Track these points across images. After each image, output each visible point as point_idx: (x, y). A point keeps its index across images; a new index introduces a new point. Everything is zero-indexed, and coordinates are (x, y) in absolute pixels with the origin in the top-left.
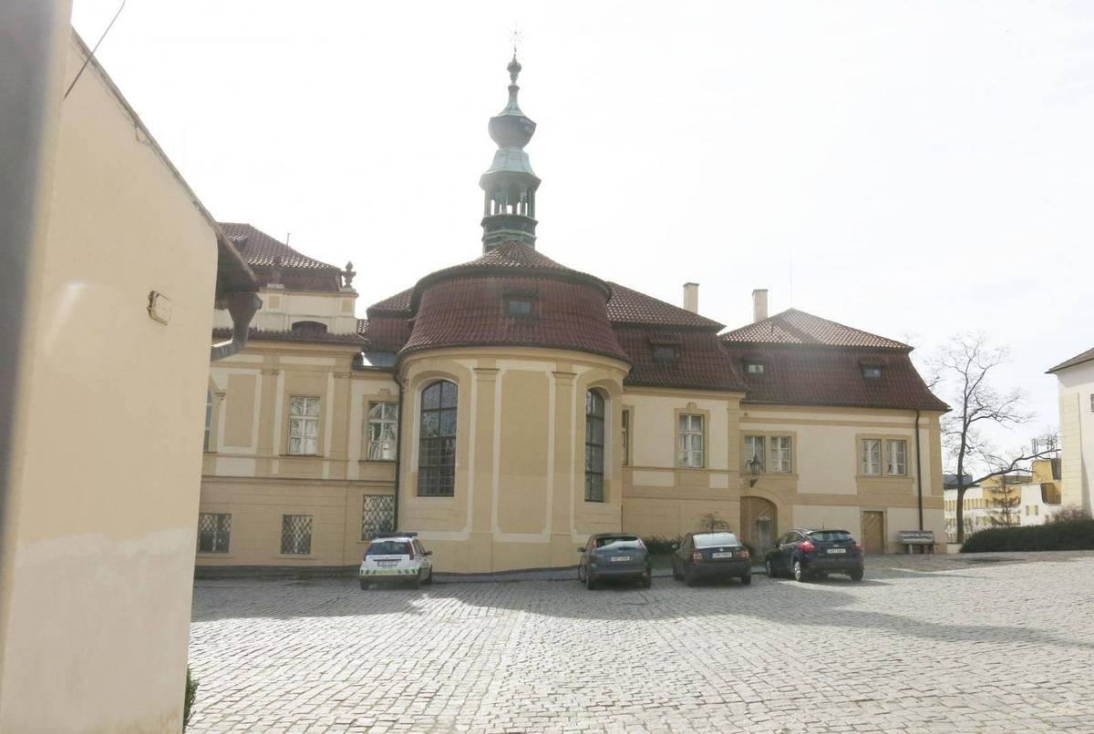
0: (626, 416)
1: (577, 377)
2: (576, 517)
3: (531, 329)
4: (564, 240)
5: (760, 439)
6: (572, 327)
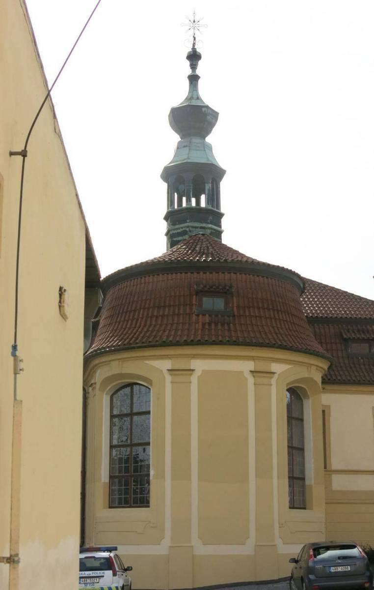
1: (276, 376)
2: (281, 526)
3: (226, 327)
4: (247, 233)
6: (254, 322)
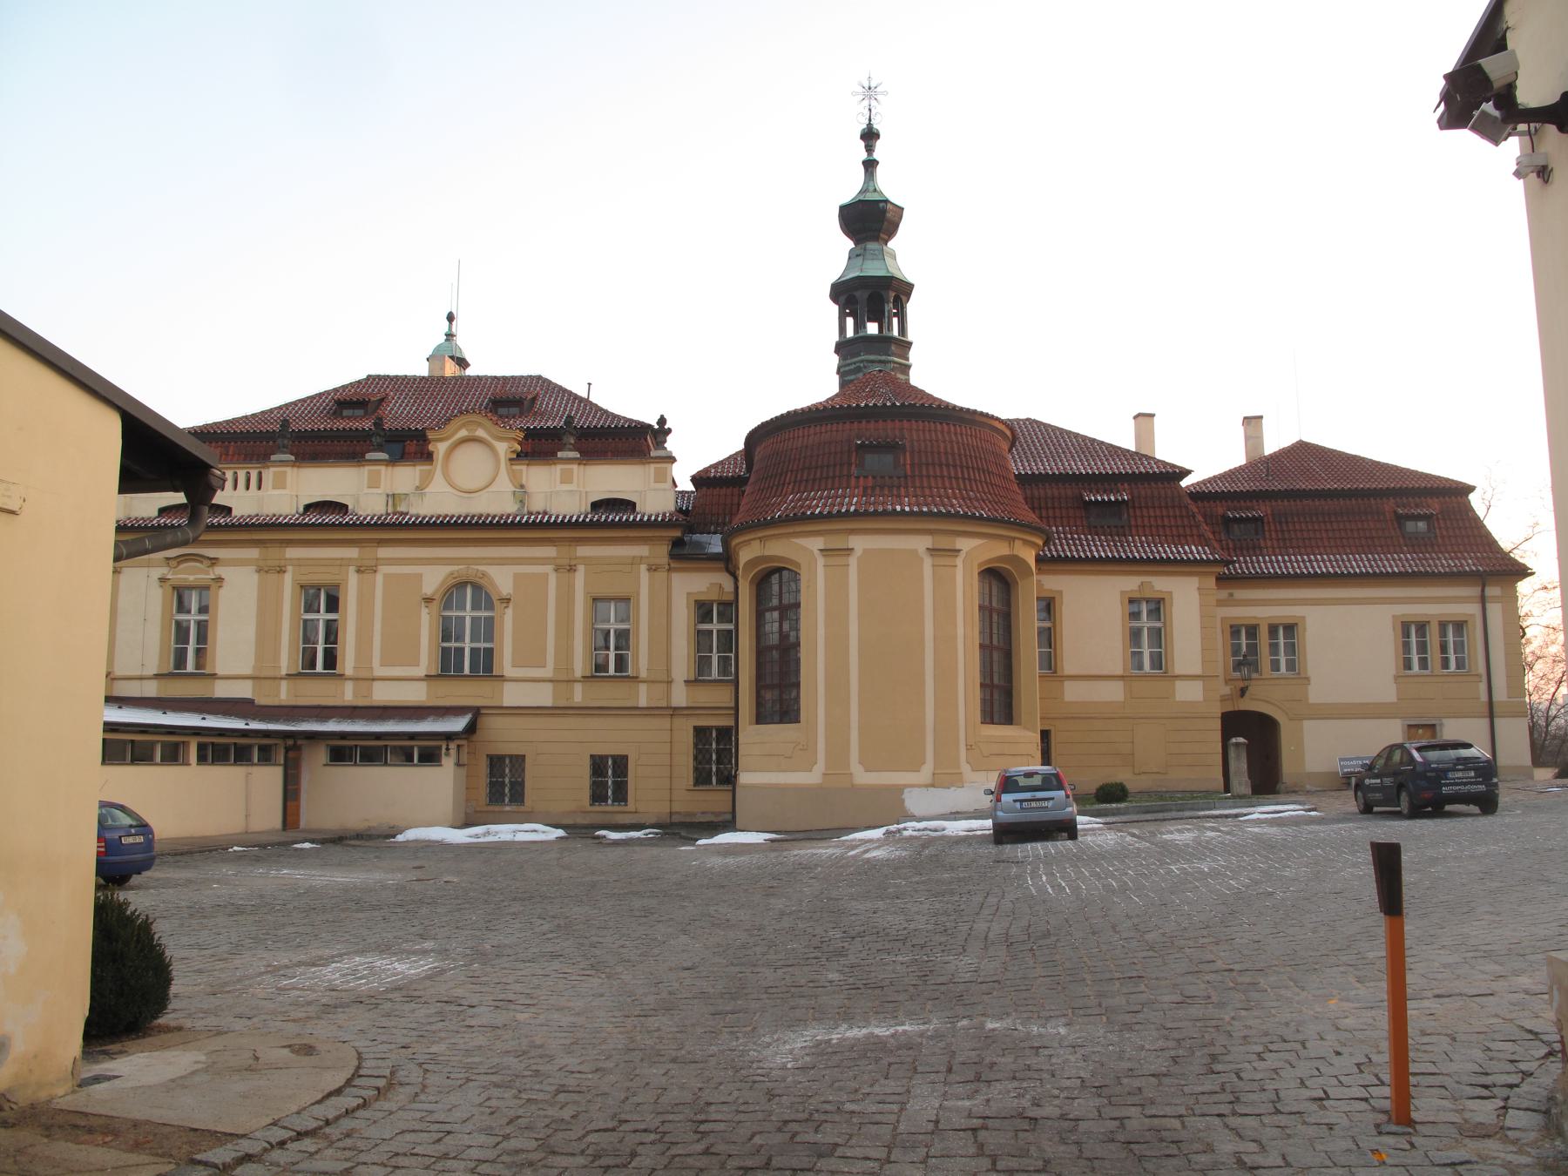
0: (1049, 606)
4: (951, 361)
5: (1252, 631)
